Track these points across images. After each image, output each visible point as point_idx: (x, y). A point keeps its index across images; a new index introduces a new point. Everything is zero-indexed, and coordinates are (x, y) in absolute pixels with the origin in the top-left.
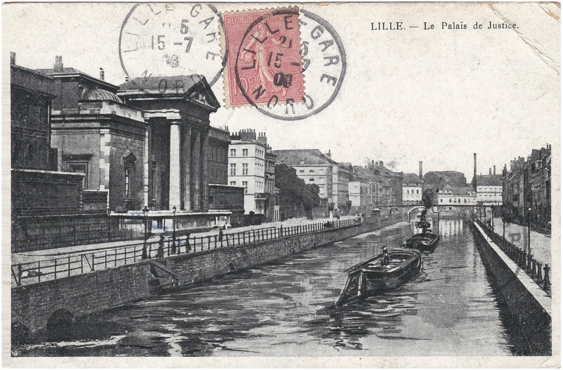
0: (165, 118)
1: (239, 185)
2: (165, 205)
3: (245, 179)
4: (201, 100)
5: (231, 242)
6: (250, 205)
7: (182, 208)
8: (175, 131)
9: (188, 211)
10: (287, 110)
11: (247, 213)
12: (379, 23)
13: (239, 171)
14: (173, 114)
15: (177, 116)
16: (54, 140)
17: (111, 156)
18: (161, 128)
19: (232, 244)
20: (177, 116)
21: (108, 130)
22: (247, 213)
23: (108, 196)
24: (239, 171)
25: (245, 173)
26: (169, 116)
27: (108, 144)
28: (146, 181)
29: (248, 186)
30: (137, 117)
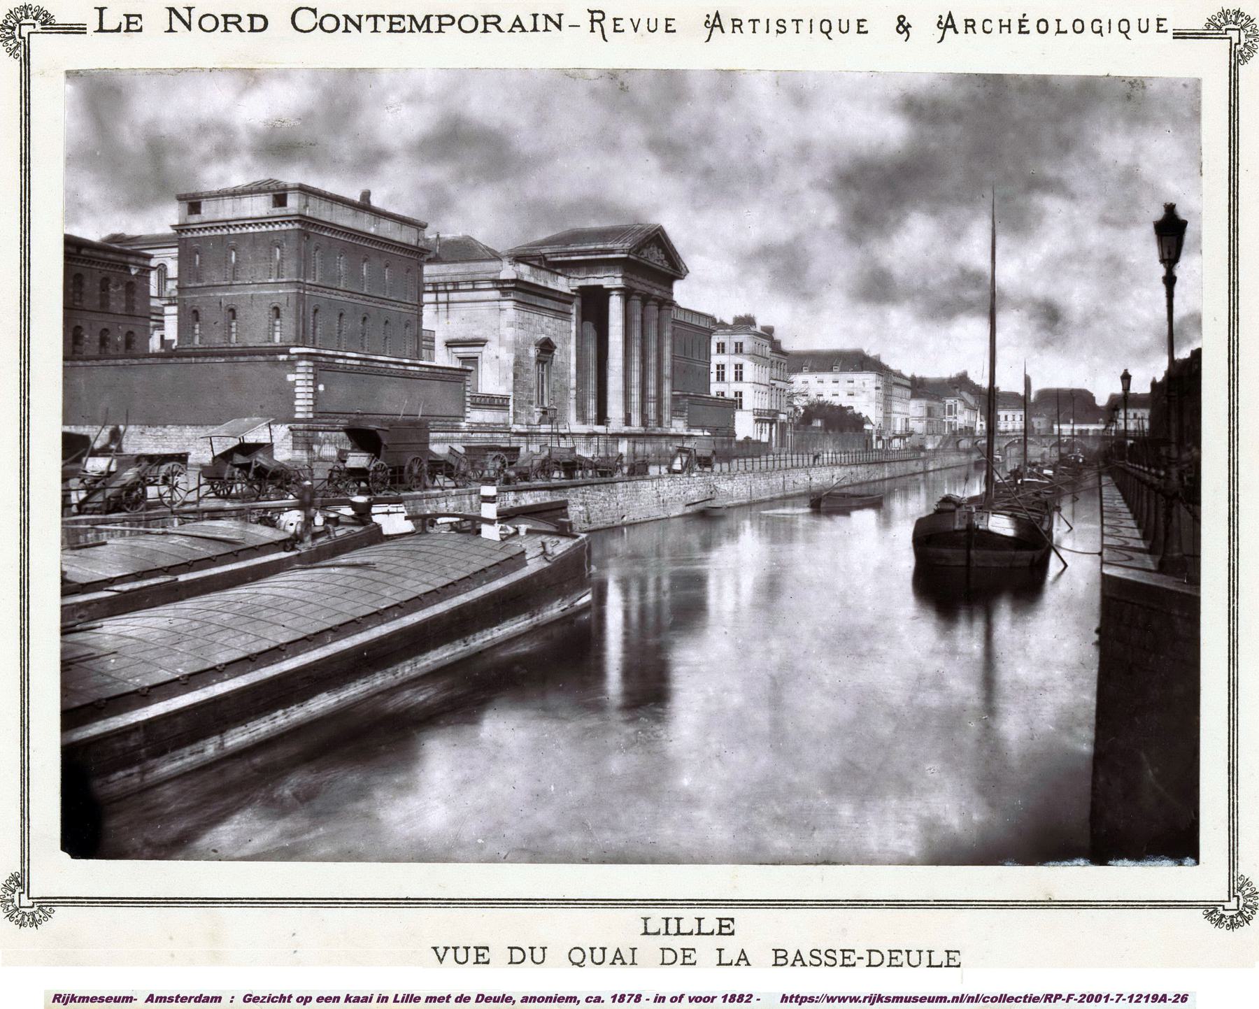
0: (601, 286)
1: (730, 395)
2: (602, 418)
3: (738, 387)
4: (655, 257)
5: (741, 465)
6: (745, 426)
7: (628, 421)
8: (616, 305)
9: (636, 426)
10: (1171, 256)
11: (740, 437)
12: (535, 16)
13: (730, 374)
14: (611, 280)
15: (619, 283)
16: (429, 318)
17: (516, 342)
18: (593, 305)
19: (1122, 427)
20: (619, 283)
21: (512, 303)
22: (740, 437)
23: (511, 402)
24: (730, 374)
25: (739, 377)
26: (606, 283)
27: (511, 325)
28: (573, 383)
29: (744, 398)
30: (563, 284)
